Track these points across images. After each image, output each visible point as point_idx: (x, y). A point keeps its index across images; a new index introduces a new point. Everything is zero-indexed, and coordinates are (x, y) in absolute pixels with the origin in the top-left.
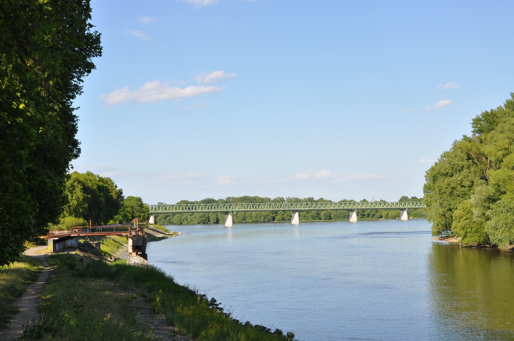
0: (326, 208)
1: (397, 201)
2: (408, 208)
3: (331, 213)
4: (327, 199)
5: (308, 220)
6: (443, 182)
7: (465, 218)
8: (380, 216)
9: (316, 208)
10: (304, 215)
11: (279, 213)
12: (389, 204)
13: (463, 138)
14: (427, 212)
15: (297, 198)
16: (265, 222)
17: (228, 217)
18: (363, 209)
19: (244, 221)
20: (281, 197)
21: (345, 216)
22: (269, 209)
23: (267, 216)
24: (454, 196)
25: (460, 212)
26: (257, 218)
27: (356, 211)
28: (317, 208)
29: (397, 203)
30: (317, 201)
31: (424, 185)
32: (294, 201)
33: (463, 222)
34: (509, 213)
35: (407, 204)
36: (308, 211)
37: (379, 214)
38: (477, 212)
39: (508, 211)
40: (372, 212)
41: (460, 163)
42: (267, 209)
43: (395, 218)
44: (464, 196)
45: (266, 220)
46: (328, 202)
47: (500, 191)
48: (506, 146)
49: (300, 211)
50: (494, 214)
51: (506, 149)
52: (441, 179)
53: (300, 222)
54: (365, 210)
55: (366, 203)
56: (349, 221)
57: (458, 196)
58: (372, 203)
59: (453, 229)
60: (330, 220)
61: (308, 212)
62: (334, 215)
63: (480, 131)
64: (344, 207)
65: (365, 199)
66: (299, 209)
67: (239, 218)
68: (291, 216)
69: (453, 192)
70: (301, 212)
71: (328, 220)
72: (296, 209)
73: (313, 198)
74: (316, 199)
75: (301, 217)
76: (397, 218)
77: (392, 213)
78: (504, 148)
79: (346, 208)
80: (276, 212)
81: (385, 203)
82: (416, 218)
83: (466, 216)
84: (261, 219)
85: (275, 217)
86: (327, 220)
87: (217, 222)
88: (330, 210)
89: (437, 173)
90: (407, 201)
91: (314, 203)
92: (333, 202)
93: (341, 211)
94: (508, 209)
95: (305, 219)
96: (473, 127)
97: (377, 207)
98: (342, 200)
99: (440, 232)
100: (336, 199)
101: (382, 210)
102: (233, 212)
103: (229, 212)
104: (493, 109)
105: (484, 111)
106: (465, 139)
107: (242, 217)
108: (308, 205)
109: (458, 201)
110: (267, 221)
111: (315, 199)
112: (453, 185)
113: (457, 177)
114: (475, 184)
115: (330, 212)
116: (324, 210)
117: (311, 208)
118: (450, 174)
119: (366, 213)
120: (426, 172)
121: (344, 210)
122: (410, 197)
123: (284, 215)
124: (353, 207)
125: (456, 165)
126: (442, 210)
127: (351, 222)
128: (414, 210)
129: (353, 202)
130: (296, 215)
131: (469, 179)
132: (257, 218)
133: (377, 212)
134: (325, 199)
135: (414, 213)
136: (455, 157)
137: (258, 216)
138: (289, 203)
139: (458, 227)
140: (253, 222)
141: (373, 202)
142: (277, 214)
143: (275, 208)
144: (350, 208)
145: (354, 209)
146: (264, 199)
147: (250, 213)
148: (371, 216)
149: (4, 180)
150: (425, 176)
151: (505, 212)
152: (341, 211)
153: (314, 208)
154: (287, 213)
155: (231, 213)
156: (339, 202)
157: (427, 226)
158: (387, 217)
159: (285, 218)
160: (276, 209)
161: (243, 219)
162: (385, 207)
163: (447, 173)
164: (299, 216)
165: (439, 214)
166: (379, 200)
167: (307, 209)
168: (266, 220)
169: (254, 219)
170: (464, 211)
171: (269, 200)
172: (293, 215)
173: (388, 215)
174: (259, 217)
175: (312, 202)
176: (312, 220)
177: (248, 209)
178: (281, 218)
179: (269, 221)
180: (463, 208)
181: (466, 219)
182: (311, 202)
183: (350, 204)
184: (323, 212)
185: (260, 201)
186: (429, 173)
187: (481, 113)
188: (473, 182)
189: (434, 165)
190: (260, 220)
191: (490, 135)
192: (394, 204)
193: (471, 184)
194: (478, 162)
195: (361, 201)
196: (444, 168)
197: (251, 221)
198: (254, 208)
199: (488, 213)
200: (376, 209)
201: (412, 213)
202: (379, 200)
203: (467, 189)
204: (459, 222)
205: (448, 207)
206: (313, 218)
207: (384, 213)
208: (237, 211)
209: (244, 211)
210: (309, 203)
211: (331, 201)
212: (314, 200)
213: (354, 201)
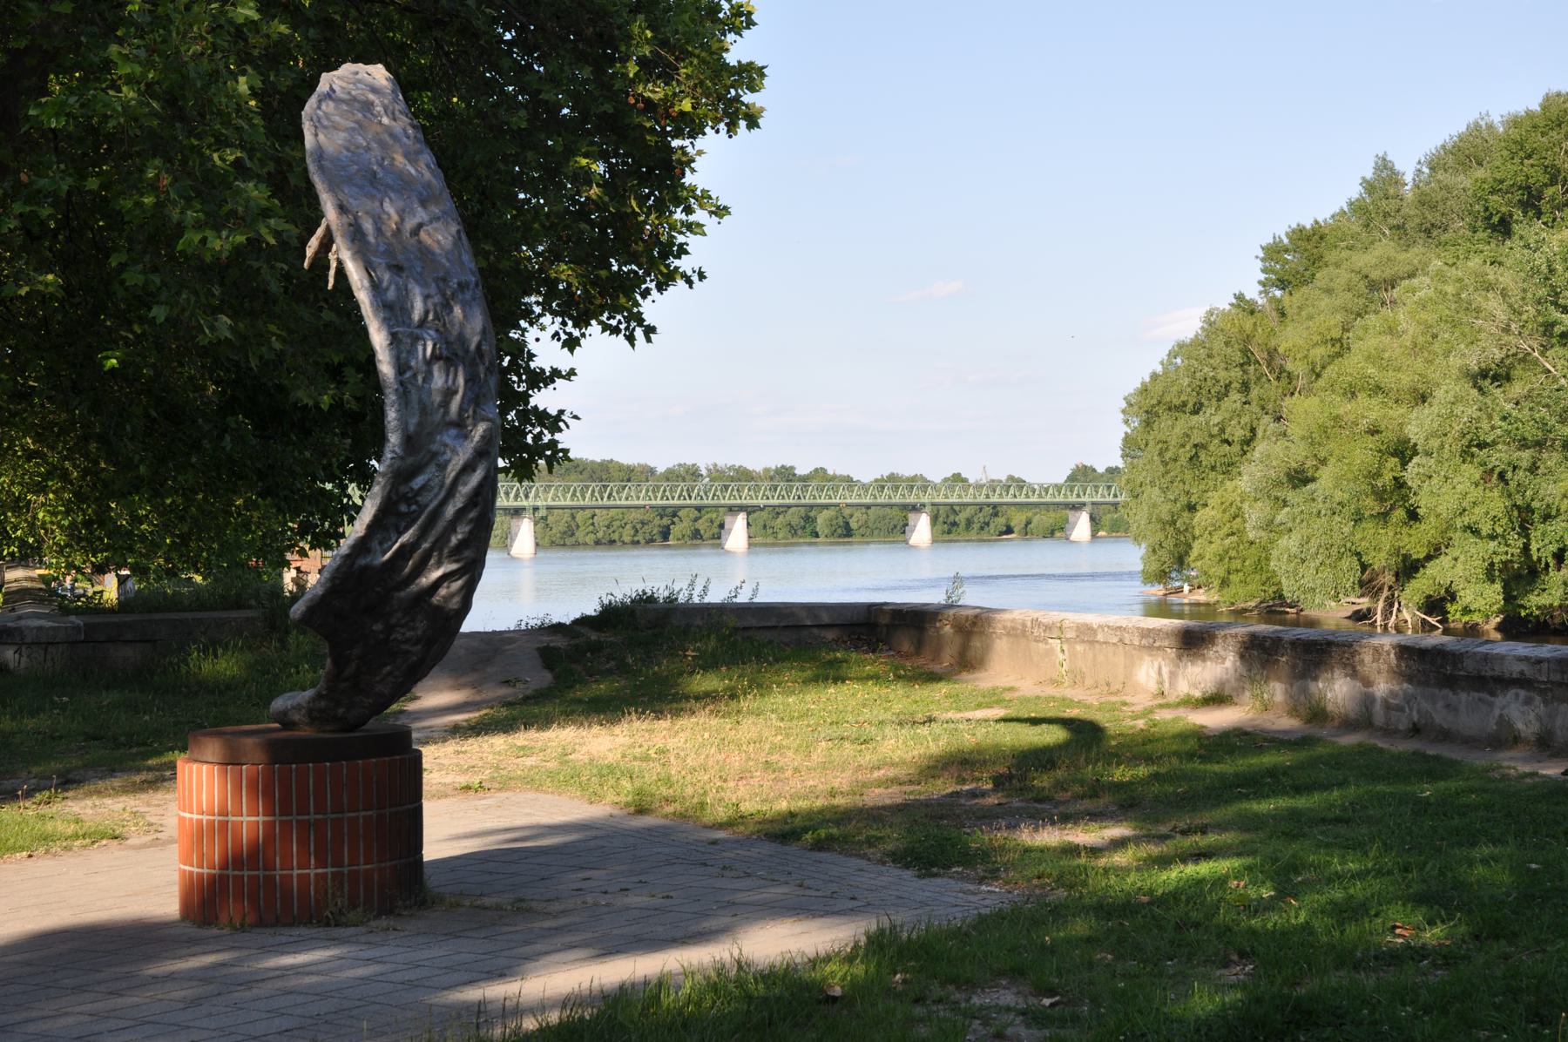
0: (834, 501)
1: (1061, 478)
2: (1093, 503)
3: (851, 516)
4: (838, 473)
5: (776, 538)
6: (1173, 429)
7: (1225, 530)
8: (1005, 528)
9: (803, 501)
10: (762, 523)
11: (680, 513)
12: (1034, 491)
13: (1234, 301)
14: (1131, 513)
15: (740, 467)
16: (638, 542)
17: (918, 520)
18: (951, 505)
19: (569, 541)
20: (689, 463)
21: (895, 526)
22: (653, 502)
23: (643, 523)
24: (1202, 469)
25: (1213, 513)
26: (612, 529)
27: (928, 509)
28: (807, 501)
29: (1058, 488)
30: (804, 479)
31: (1123, 435)
32: (732, 477)
33: (1219, 541)
34: (1337, 519)
35: (1088, 491)
36: (777, 509)
37: (1001, 521)
38: (1255, 514)
39: (1334, 513)
40: (981, 515)
41: (1222, 375)
42: (647, 502)
43: (1052, 533)
44: (1228, 468)
45: (640, 538)
46: (841, 481)
47: (1315, 455)
48: (1336, 333)
49: (749, 510)
50: (1298, 521)
51: (1334, 341)
52: (1165, 422)
53: (750, 545)
54: (957, 508)
55: (960, 484)
56: (906, 542)
57: (1213, 468)
58: (979, 487)
59: (1194, 561)
60: (846, 540)
61: (777, 511)
62: (860, 524)
63: (1282, 284)
64: (890, 498)
65: (959, 474)
66: (748, 502)
67: (554, 531)
68: (722, 526)
69: (1198, 457)
70: (754, 512)
71: (841, 540)
72: (739, 501)
73: (792, 468)
74: (801, 471)
75: (753, 529)
76: (1058, 534)
77: (1042, 519)
78: (1329, 337)
79: (897, 499)
80: (674, 513)
81: (1022, 487)
82: (1119, 534)
83: (1228, 525)
84: (624, 534)
85: (668, 527)
86: (836, 540)
87: (1051, 533)
88: (847, 505)
89: (1154, 402)
90: (1090, 481)
91: (797, 484)
92: (858, 481)
93: (881, 512)
94: (1334, 505)
95: (766, 536)
96: (1264, 271)
97: (995, 499)
98: (886, 474)
99: (1163, 571)
100: (865, 474)
101: (1013, 508)
102: (536, 509)
103: (524, 509)
104: (1320, 220)
105: (1294, 226)
106: (1239, 306)
107: (562, 527)
108: (776, 490)
109: (1211, 483)
110: (643, 542)
111: (799, 472)
112: (1197, 438)
113: (1211, 414)
114: (1260, 433)
115: (847, 512)
116: (827, 507)
117: (787, 501)
118: (1190, 405)
119: (961, 518)
120: (1125, 399)
121: (891, 506)
122: (1101, 469)
123: (700, 521)
124: (919, 498)
125: (1208, 379)
126: (1168, 507)
127: (912, 546)
128: (1112, 508)
129: (919, 483)
130: (739, 522)
131: (1242, 422)
132: (612, 529)
133: (996, 515)
134: (830, 472)
135: (1112, 519)
136: (1209, 356)
137: (616, 524)
138: (716, 484)
139: (1207, 557)
140: (598, 543)
141: (984, 481)
142: (676, 519)
143: (690, 497)
144: (911, 500)
145: (924, 506)
146: (633, 470)
147: (588, 513)
148: (976, 526)
149: (361, 376)
150: (1124, 412)
151: (1325, 515)
152: (881, 512)
153: (796, 501)
154: (709, 515)
155: (529, 514)
156: (876, 481)
157: (1131, 555)
158: (1027, 532)
159: (702, 532)
160: (676, 502)
161: (565, 533)
162: (1021, 499)
163: (1184, 404)
164: (748, 524)
165: (1160, 520)
166: (1004, 478)
167: (775, 502)
168: (640, 538)
169: (600, 535)
170: (1224, 511)
171: (652, 471)
172: (728, 519)
173: (1032, 526)
174: (618, 527)
175: (791, 481)
176: (788, 539)
177: (587, 502)
178: (689, 533)
179: (650, 541)
180: (1222, 503)
181: (1228, 535)
182: (788, 481)
183: (912, 487)
184: (826, 514)
185: (622, 474)
186: (1133, 401)
187: (1288, 230)
188: (1253, 430)
189: (1147, 379)
190: (621, 536)
191: (1299, 295)
192: (1051, 491)
193: (1248, 434)
194: (1270, 372)
195: (946, 480)
196: (1175, 388)
197: (590, 539)
198: (605, 499)
199: (1283, 515)
200: (995, 506)
201: (1107, 519)
202: (1004, 478)
203: (1236, 448)
204: (1211, 542)
205: (1183, 500)
206: (793, 530)
207: (1018, 520)
208: (549, 508)
209: (571, 509)
210: (782, 484)
211: (849, 479)
212: (795, 475)
213: (926, 480)
